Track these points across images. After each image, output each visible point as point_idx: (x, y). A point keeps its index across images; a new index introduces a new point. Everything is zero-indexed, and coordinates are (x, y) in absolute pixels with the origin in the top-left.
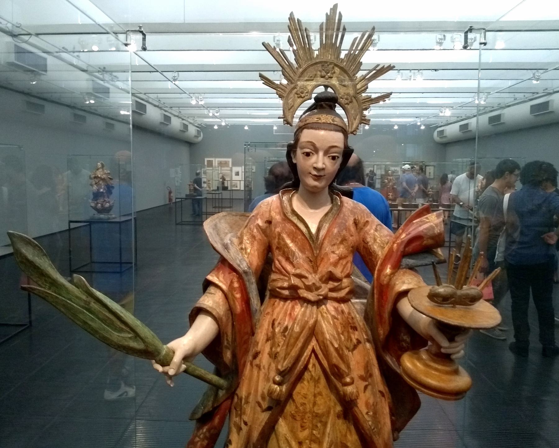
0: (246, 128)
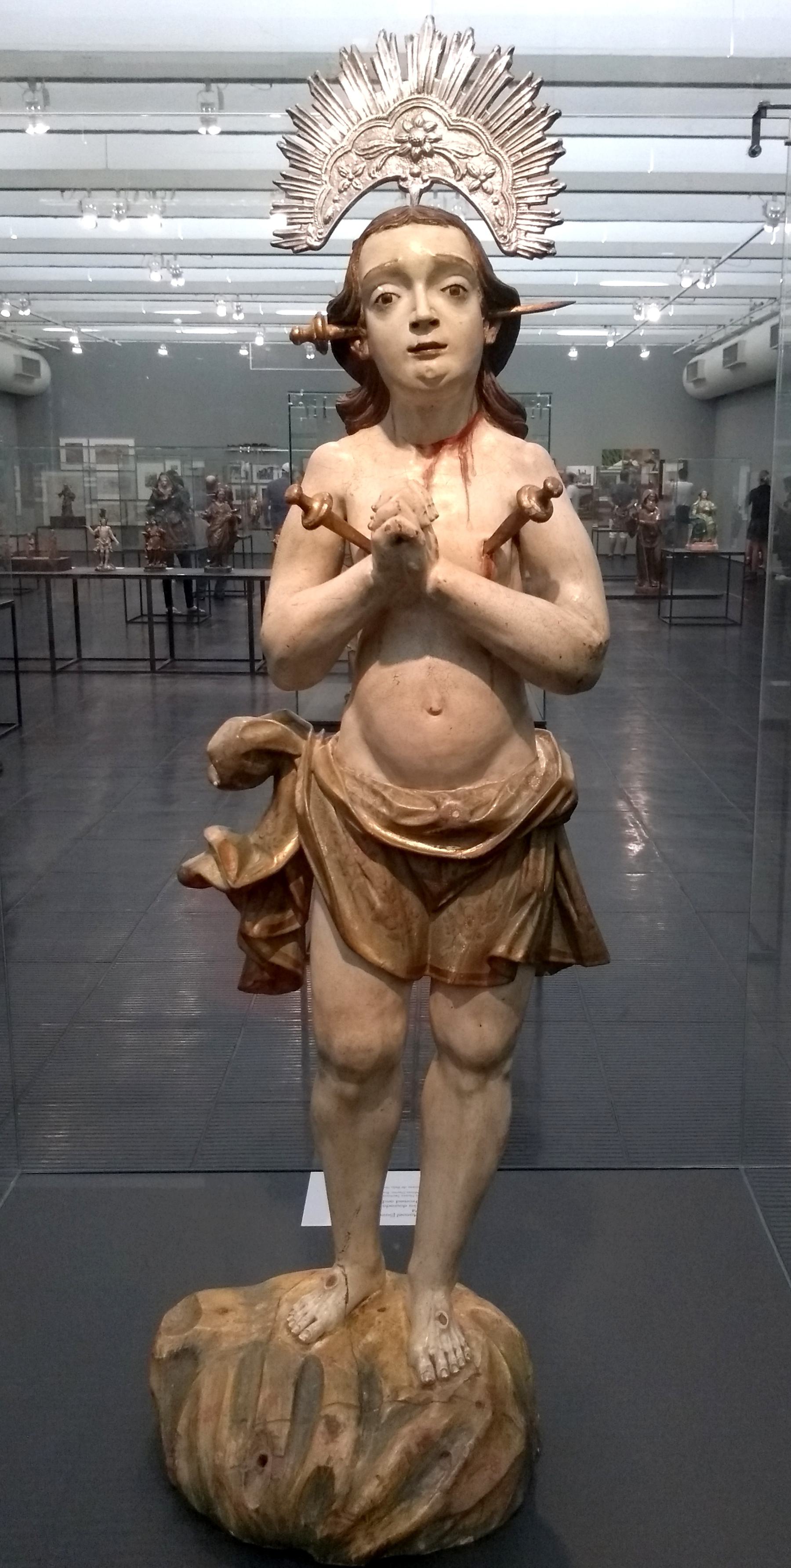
0: (163, 352)
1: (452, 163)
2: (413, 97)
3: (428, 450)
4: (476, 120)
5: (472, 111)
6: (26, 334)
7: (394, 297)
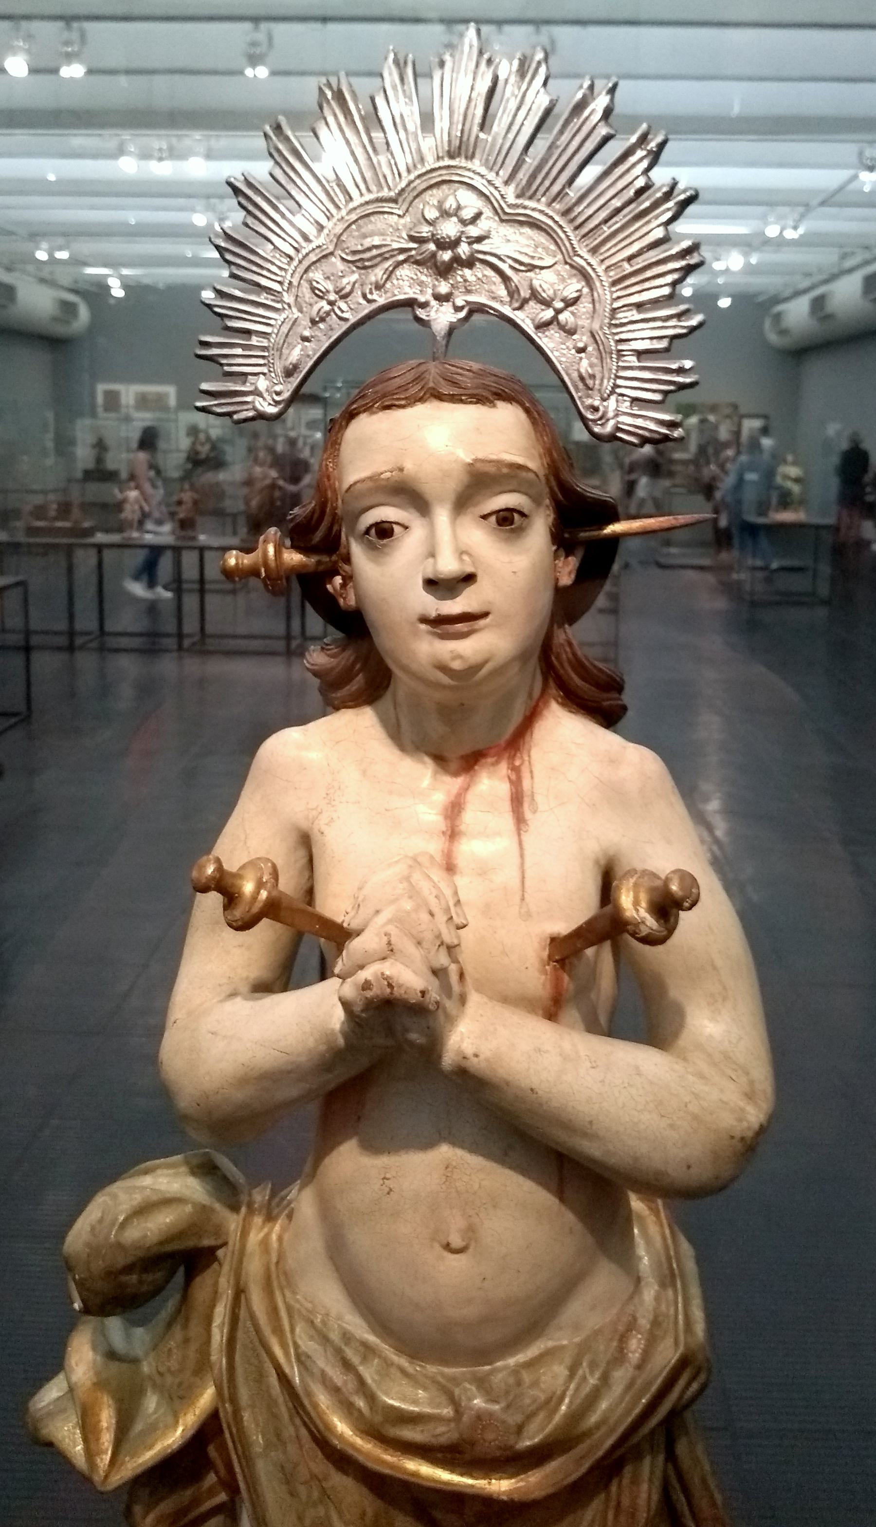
1: (505, 279)
2: (441, 164)
3: (454, 765)
4: (549, 205)
5: (542, 189)
6: (65, 277)
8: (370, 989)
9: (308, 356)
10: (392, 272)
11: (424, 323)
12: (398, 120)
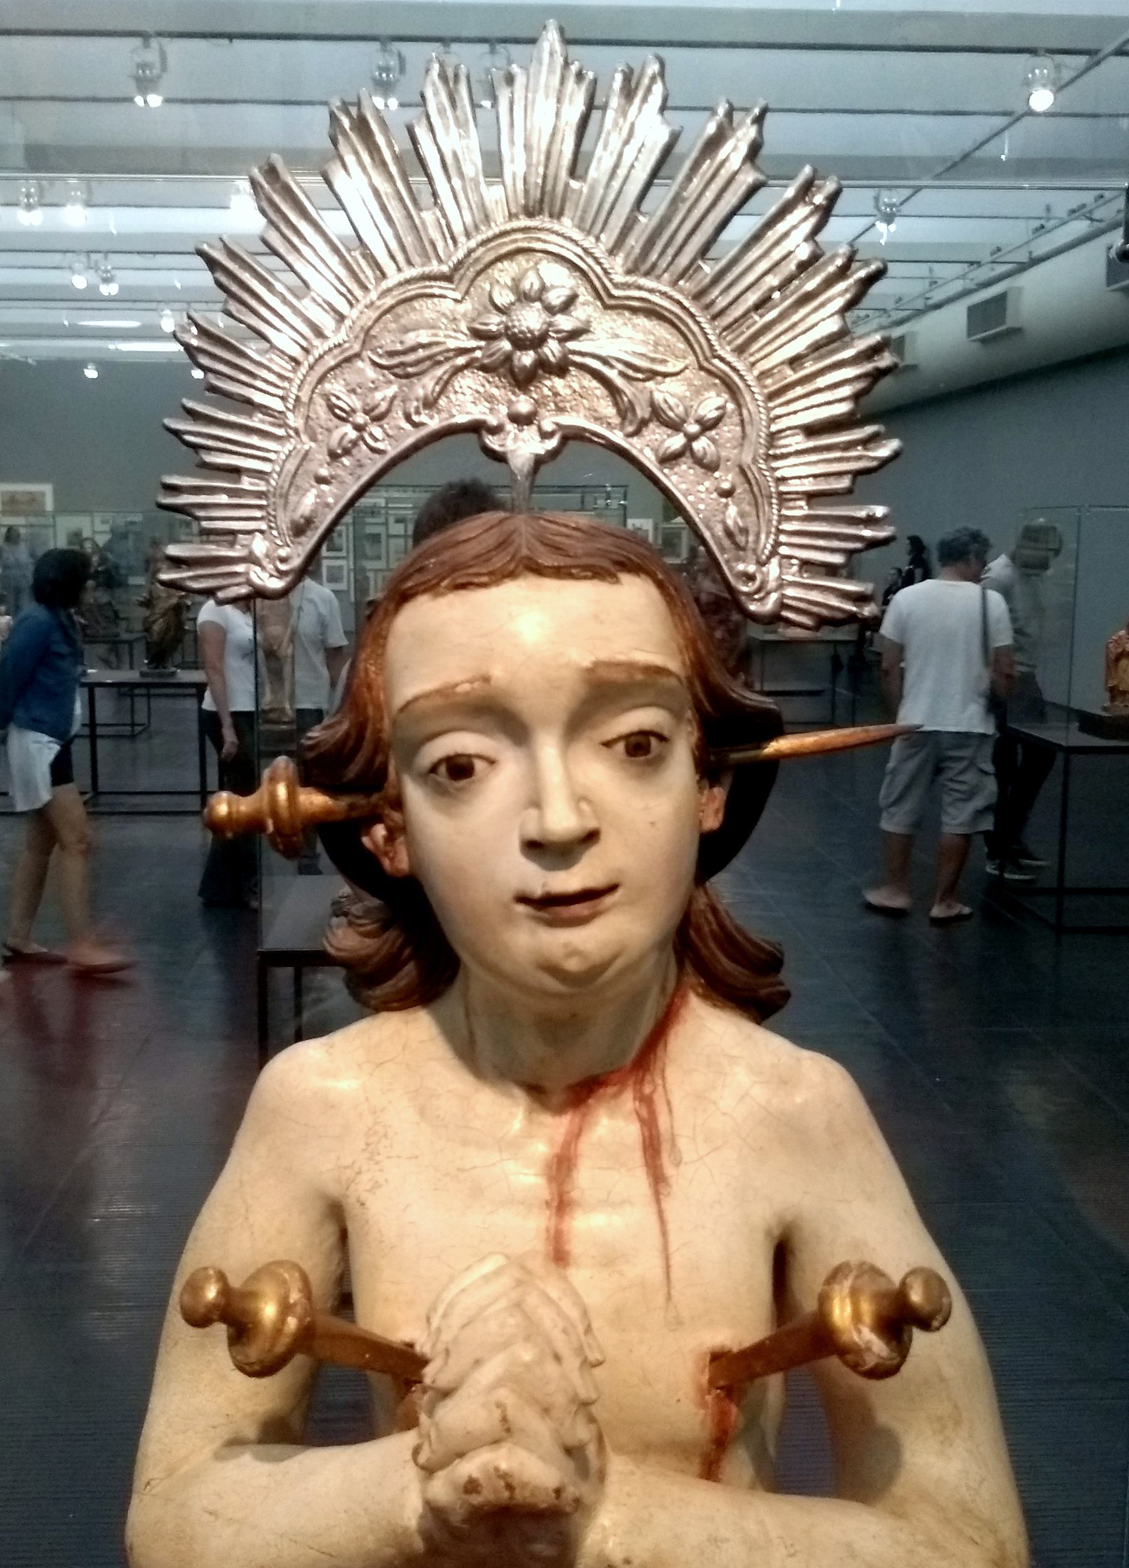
0: (91, 373)
2: (516, 224)
3: (556, 1099)
7: (479, 765)
8: (479, 1493)
9: (327, 505)
10: (447, 382)
11: (499, 458)
12: (449, 160)
